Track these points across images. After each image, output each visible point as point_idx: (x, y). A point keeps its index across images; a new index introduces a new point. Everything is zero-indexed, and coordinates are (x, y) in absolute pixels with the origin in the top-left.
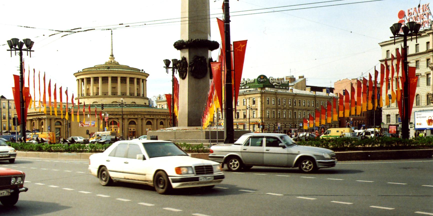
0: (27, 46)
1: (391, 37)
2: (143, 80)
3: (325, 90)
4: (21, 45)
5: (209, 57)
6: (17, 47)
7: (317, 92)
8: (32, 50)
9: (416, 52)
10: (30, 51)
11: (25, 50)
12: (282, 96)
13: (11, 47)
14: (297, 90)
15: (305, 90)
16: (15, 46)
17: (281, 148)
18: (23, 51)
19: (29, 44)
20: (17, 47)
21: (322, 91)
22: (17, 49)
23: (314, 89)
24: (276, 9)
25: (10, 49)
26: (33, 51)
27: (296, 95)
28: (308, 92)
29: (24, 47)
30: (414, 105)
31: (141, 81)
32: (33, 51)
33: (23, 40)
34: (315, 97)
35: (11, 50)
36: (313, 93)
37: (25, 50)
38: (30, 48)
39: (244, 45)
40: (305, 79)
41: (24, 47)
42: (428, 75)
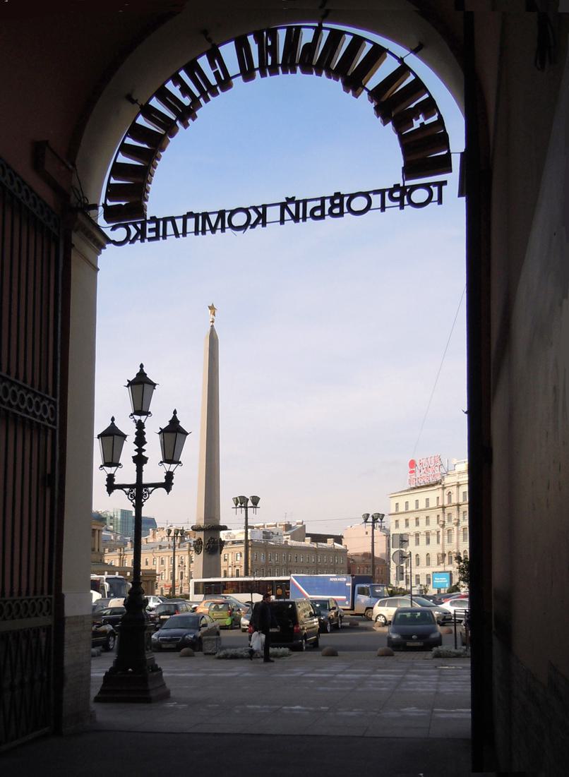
2: (99, 531)
3: (330, 541)
7: (319, 543)
9: (396, 511)
12: (274, 551)
14: (293, 541)
15: (304, 541)
19: (256, 500)
21: (326, 542)
23: (317, 538)
24: (400, 494)
25: (235, 506)
27: (292, 547)
28: (307, 543)
29: (250, 504)
30: (468, 551)
31: (97, 532)
34: (316, 551)
36: (314, 545)
38: (256, 505)
39: (42, 428)
40: (305, 526)
41: (250, 504)
42: (438, 532)
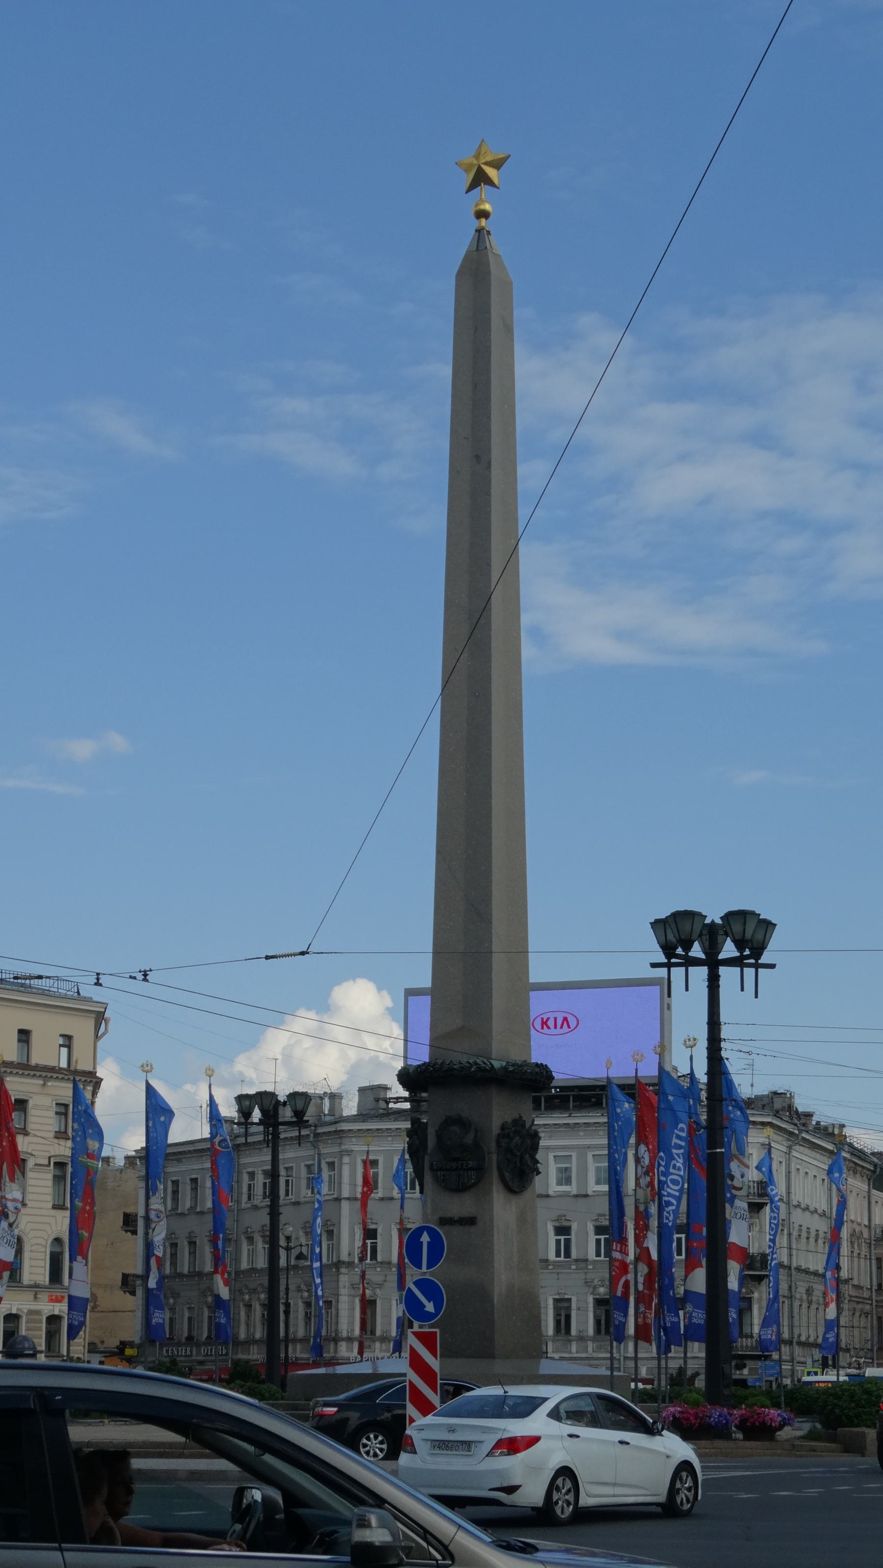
0: (740, 944)
1: (654, 965)
4: (712, 936)
5: (302, 1012)
6: (697, 951)
8: (763, 960)
10: (757, 966)
11: (730, 962)
13: (668, 949)
16: (687, 947)
17: (360, 1244)
18: (723, 970)
20: (697, 951)
22: (696, 962)
26: (772, 966)
29: (729, 950)
32: (772, 966)
33: (721, 918)
35: (669, 965)
37: (730, 962)
38: (758, 950)
41: (729, 950)
